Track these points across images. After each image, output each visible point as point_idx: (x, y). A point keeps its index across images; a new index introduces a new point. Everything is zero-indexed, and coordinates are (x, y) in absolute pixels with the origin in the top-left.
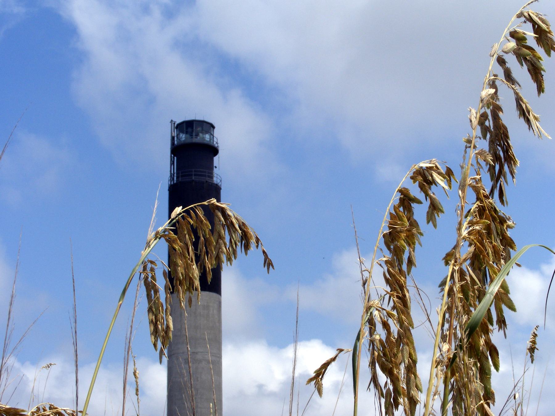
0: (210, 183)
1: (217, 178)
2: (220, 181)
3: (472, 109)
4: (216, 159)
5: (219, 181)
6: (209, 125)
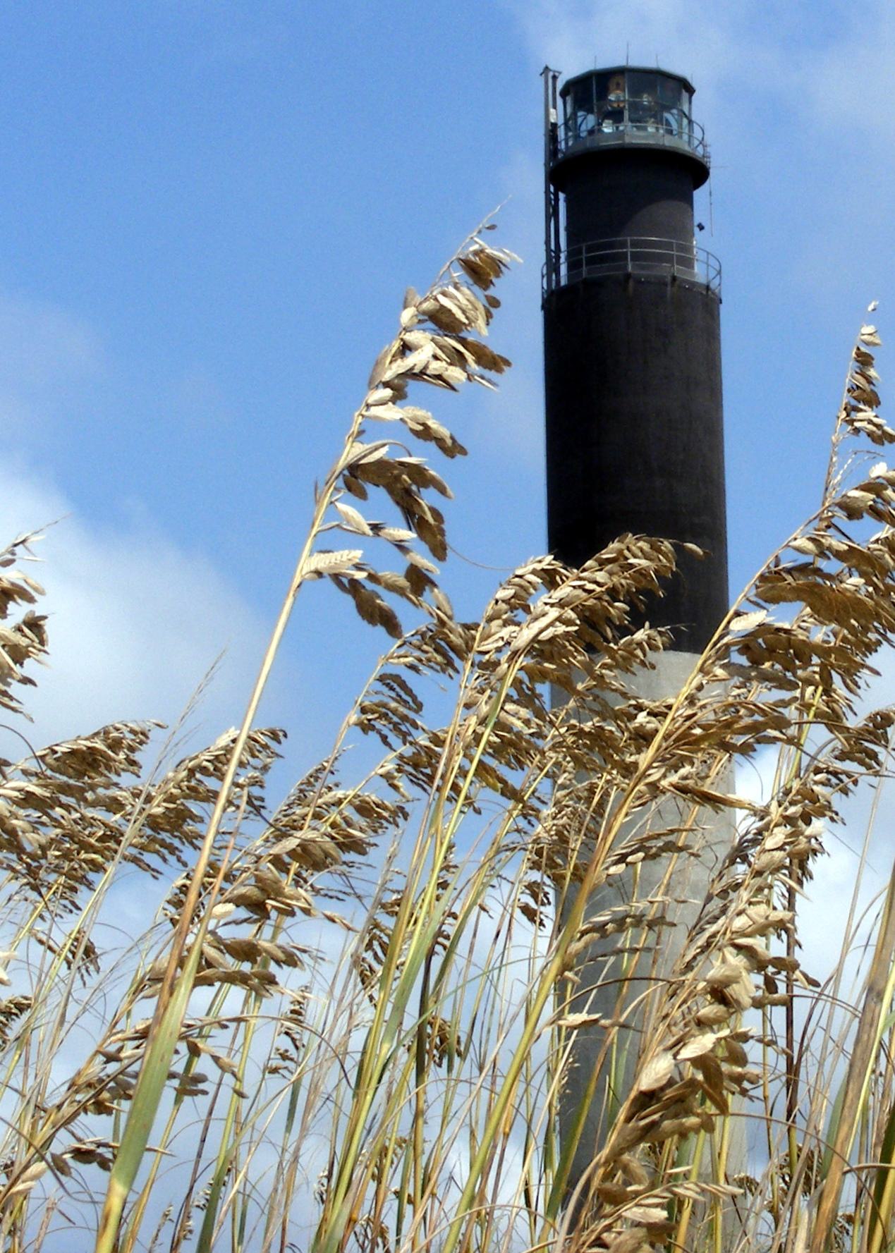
4: (699, 195)
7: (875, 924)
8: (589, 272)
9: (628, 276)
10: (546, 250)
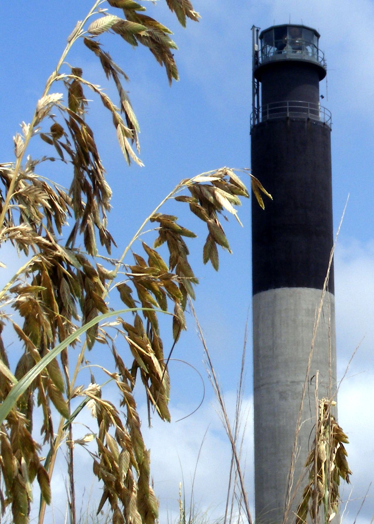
0: (314, 121)
1: (324, 113)
2: (329, 118)
3: (26, 125)
4: (322, 83)
5: (327, 118)
6: (311, 32)
7: (339, 386)
8: (270, 116)
9: (288, 118)
10: (253, 108)
